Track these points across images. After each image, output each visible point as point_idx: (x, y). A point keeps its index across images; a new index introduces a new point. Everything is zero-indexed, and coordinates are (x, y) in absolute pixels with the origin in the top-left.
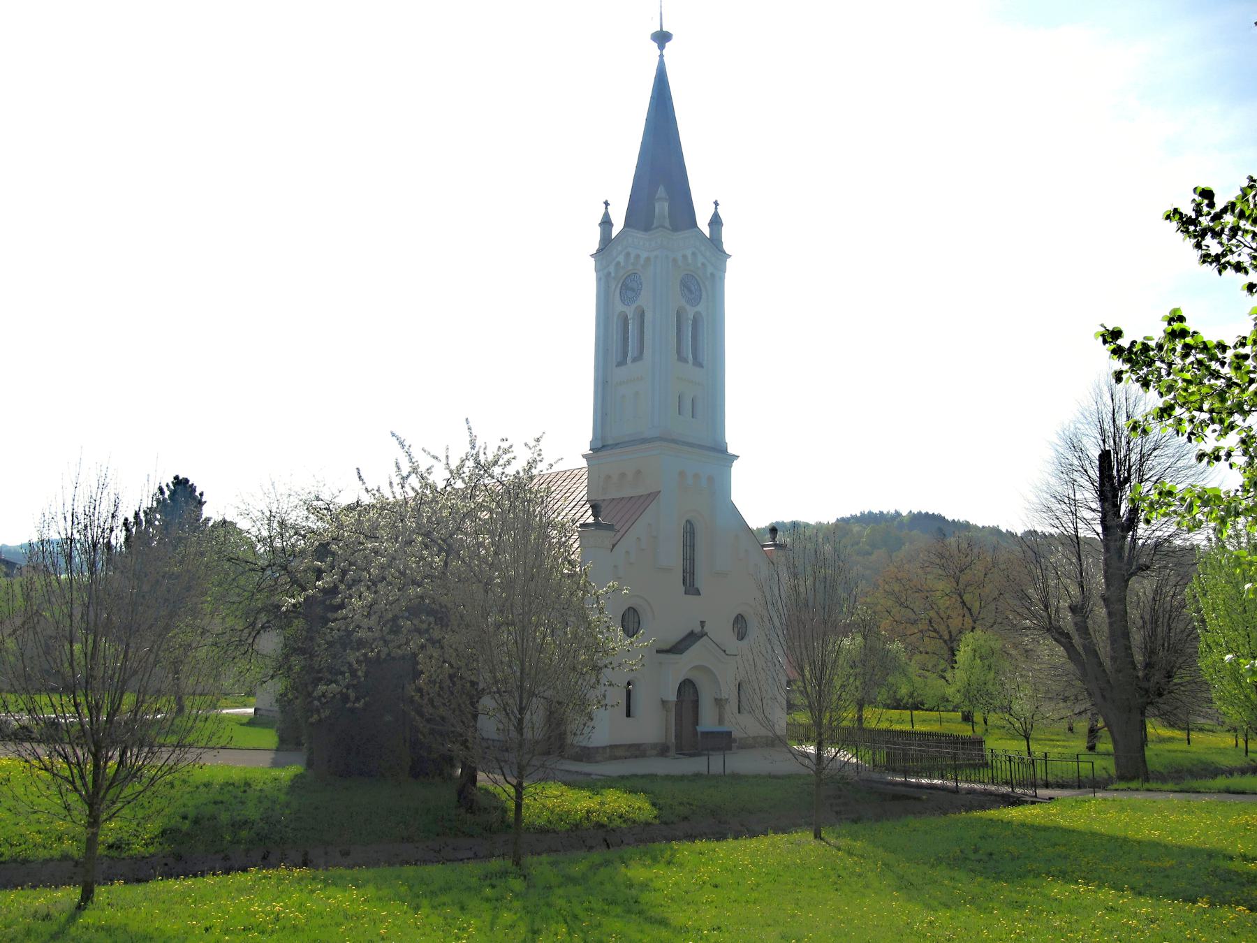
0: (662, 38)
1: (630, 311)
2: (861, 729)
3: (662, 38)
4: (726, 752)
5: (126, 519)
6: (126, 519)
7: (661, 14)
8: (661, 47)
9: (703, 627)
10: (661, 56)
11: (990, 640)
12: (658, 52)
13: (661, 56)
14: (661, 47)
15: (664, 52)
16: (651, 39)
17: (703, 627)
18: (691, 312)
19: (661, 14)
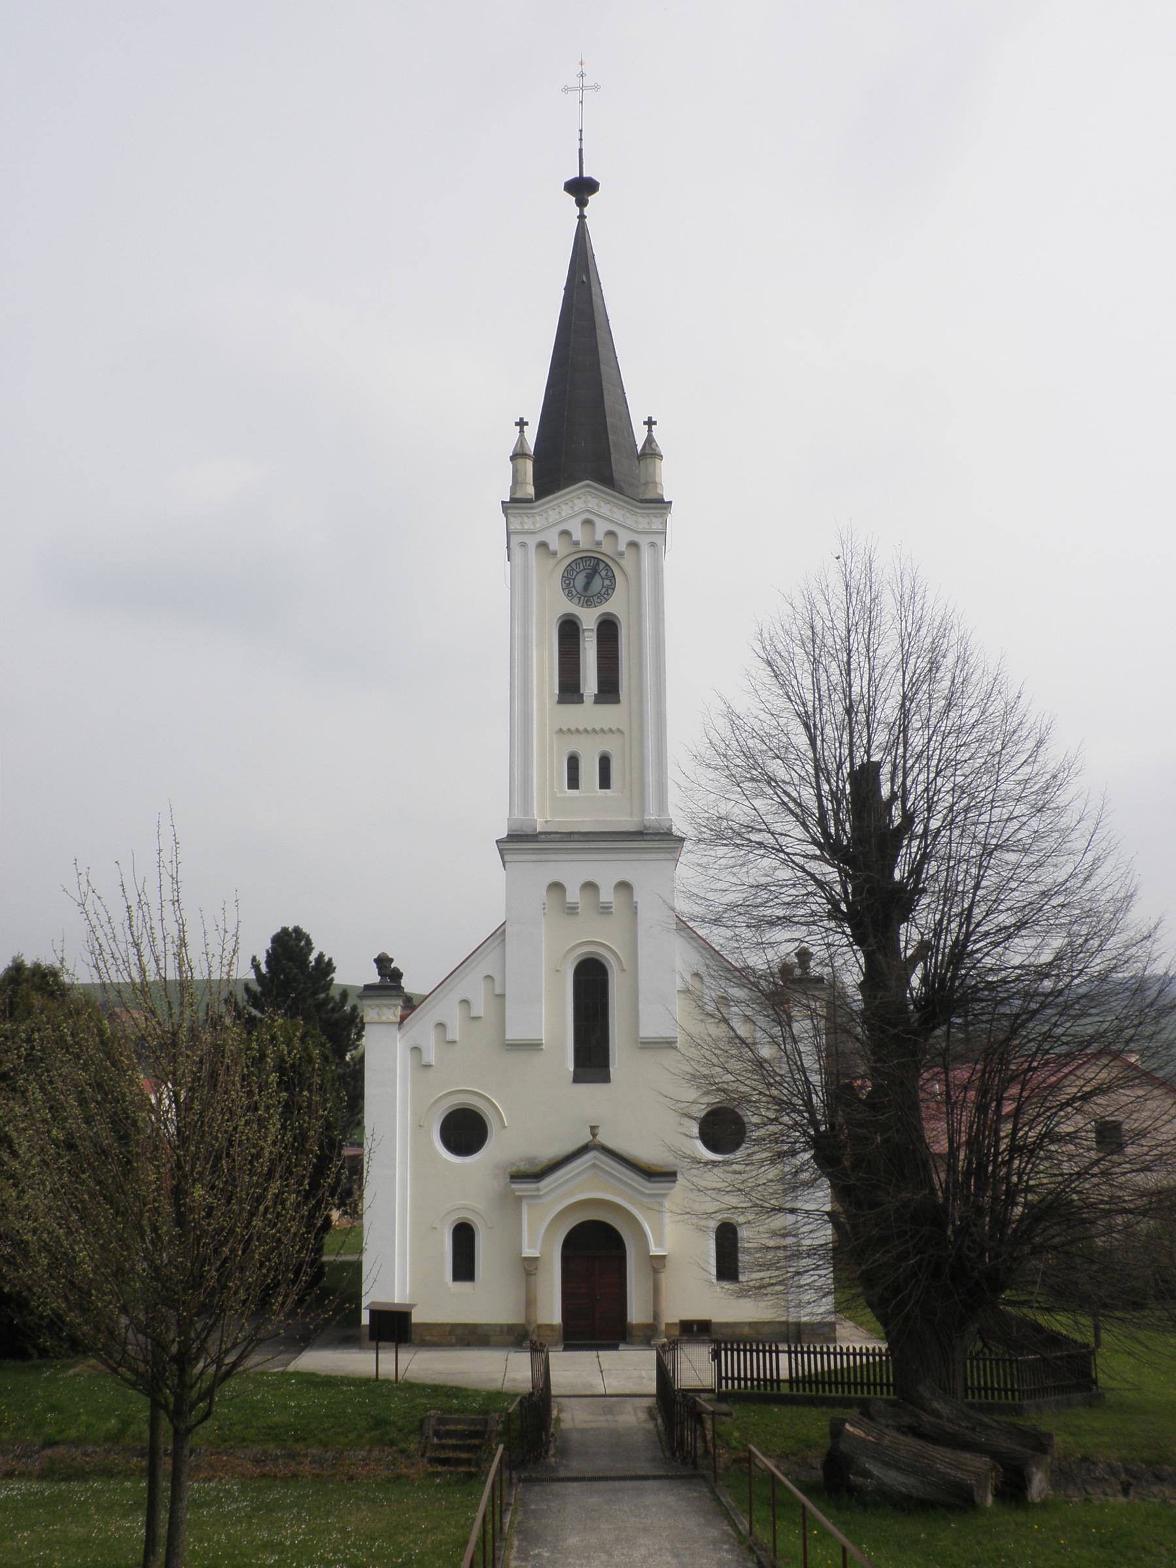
0: (582, 188)
1: (589, 619)
2: (1095, 1315)
3: (582, 188)
4: (381, 1344)
5: (254, 959)
6: (254, 959)
7: (581, 151)
8: (582, 203)
9: (594, 1135)
10: (582, 217)
11: (157, 1167)
12: (577, 210)
13: (582, 217)
14: (582, 203)
15: (587, 211)
16: (565, 189)
17: (594, 1135)
18: (589, 619)
19: (581, 151)
